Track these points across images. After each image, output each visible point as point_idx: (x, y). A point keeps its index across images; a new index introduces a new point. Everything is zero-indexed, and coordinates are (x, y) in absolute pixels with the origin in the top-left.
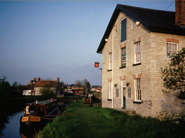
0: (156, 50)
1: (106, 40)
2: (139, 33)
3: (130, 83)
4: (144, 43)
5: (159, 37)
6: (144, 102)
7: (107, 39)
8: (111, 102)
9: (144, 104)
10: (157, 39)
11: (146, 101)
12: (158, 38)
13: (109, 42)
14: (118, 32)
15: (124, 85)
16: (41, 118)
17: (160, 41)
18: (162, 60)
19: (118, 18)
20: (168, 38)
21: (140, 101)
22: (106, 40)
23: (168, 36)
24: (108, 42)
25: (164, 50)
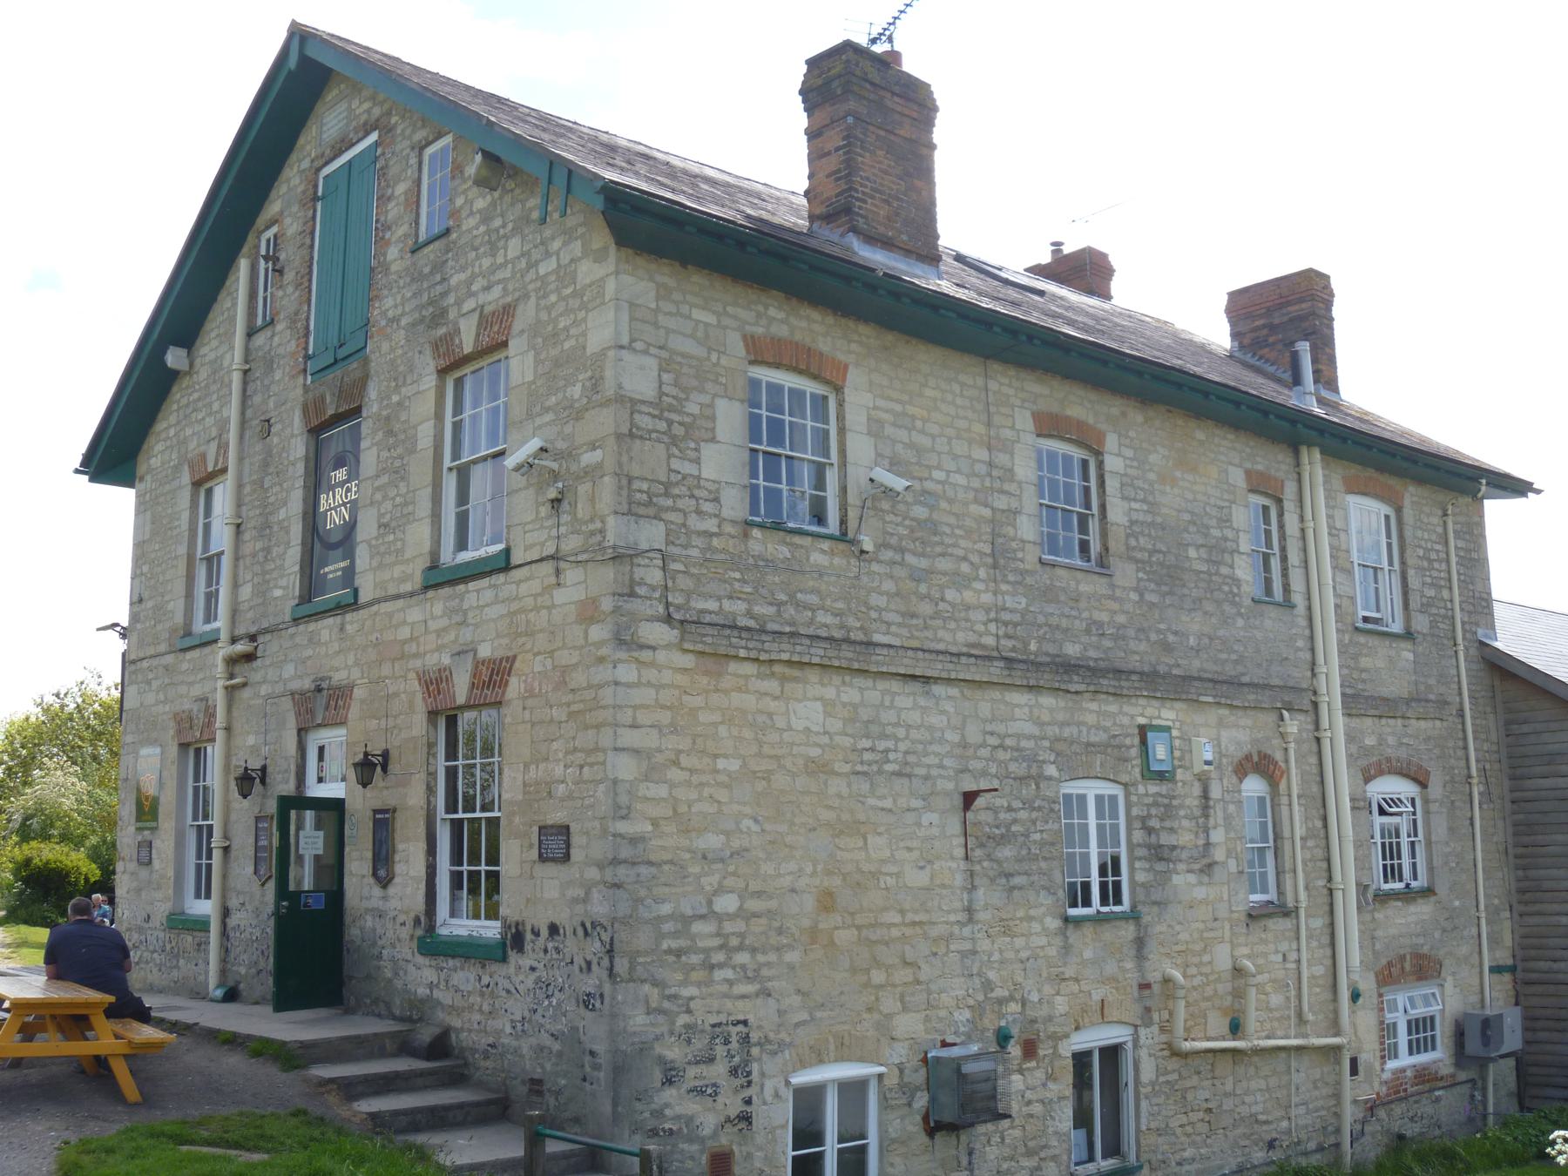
0: (662, 426)
1: (174, 358)
2: (494, 268)
3: (394, 754)
4: (537, 362)
5: (685, 309)
6: (529, 936)
7: (182, 352)
8: (202, 946)
9: (526, 962)
10: (671, 323)
11: (554, 929)
12: (679, 314)
13: (203, 374)
14: (289, 276)
15: (1068, 797)
16: (1107, 296)
17: (689, 347)
18: (711, 525)
19: (294, 157)
20: (760, 330)
21: (490, 930)
22: (174, 358)
23: (759, 316)
24: (189, 373)
25: (722, 431)
